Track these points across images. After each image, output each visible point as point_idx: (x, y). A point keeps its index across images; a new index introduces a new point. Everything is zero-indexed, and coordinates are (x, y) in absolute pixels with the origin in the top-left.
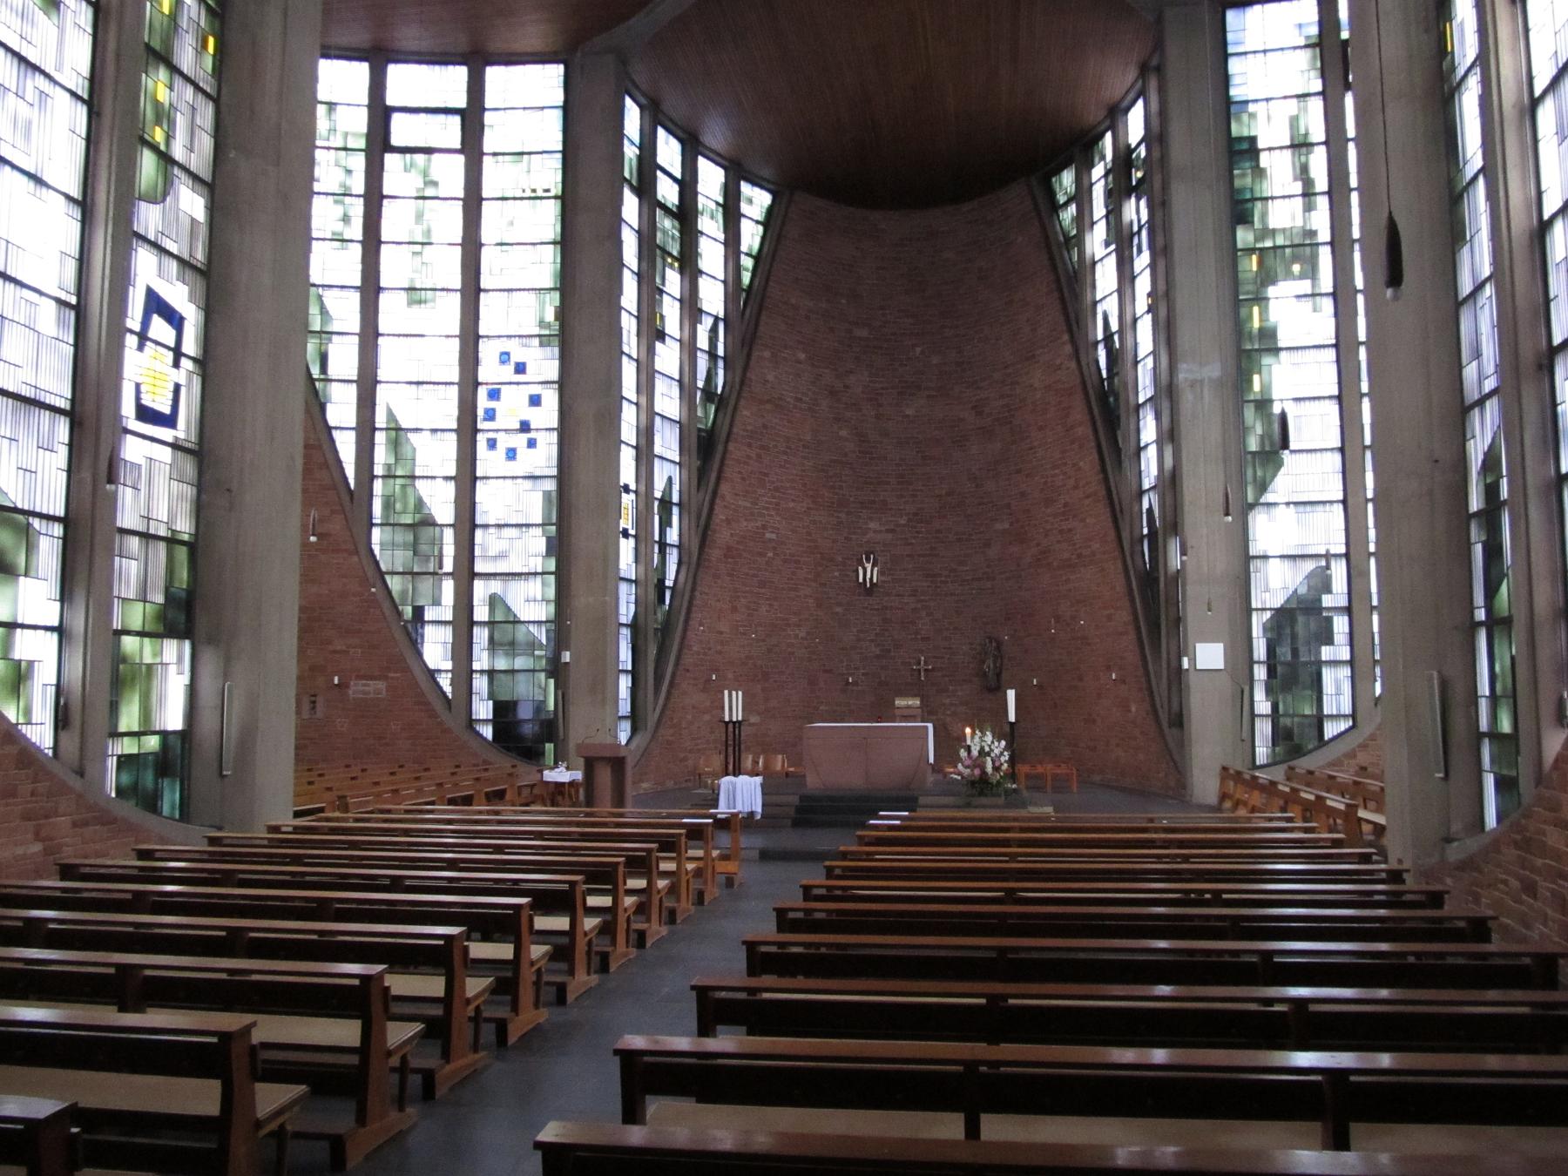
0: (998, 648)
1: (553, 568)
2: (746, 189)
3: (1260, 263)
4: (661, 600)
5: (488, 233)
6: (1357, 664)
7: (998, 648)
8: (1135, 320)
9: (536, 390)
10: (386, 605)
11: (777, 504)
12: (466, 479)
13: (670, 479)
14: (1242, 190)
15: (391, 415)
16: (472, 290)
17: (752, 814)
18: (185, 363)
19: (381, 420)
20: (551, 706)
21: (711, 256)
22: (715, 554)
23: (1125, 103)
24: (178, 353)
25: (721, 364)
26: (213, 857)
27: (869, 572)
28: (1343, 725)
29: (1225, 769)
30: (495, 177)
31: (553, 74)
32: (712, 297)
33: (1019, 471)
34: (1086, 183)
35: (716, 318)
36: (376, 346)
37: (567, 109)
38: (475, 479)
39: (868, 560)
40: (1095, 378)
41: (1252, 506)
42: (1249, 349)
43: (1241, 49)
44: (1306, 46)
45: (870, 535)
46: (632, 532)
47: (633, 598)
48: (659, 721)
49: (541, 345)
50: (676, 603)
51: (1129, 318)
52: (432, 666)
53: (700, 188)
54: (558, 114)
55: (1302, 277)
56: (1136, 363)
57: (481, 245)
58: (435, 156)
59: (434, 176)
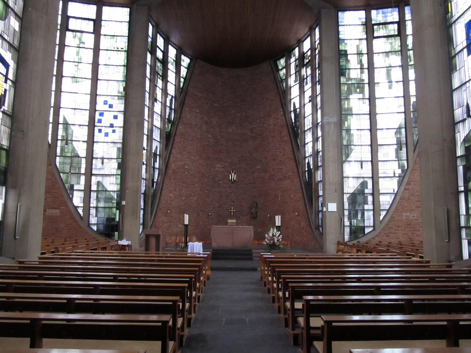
0: (257, 205)
1: (120, 173)
2: (183, 57)
3: (348, 88)
5: (102, 60)
6: (375, 211)
7: (257, 205)
8: (304, 105)
9: (116, 114)
10: (60, 184)
12: (91, 142)
13: (157, 147)
14: (342, 66)
15: (65, 119)
16: (95, 79)
18: (9, 82)
19: (61, 120)
20: (117, 219)
21: (171, 76)
22: (170, 172)
23: (303, 39)
24: (6, 78)
25: (173, 111)
26: (20, 268)
27: (233, 176)
28: (371, 229)
29: (339, 242)
30: (104, 43)
31: (126, 11)
32: (171, 90)
33: (265, 150)
34: (289, 63)
35: (172, 96)
36: (60, 95)
37: (130, 23)
38: (94, 142)
39: (233, 172)
40: (291, 122)
41: (345, 161)
42: (343, 114)
43: (343, 24)
44: (362, 25)
46: (145, 163)
49: (118, 99)
51: (303, 104)
52: (76, 205)
53: (169, 55)
54: (127, 24)
55: (360, 93)
57: (99, 65)
58: (84, 34)
59: (83, 40)
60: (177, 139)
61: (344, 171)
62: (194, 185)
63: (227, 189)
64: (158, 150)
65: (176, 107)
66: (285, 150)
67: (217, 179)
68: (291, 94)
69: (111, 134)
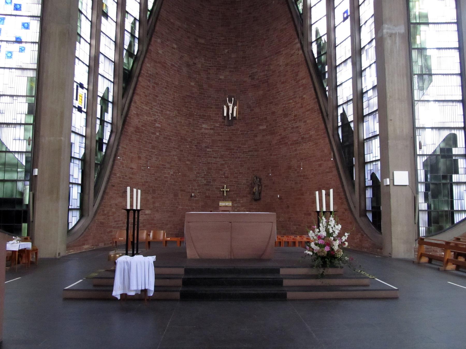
0: (260, 181)
4: (101, 149)
7: (260, 181)
8: (335, 27)
11: (162, 111)
13: (108, 89)
17: (145, 291)
22: (131, 129)
25: (137, 41)
27: (231, 109)
33: (271, 103)
35: (135, 19)
39: (230, 101)
40: (312, 58)
45: (203, 130)
47: (84, 145)
48: (96, 211)
50: (109, 151)
51: (332, 26)
56: (335, 47)
60: (143, 82)
61: (416, 117)
62: (170, 152)
63: (218, 160)
64: (111, 95)
65: (141, 35)
66: (304, 98)
67: (204, 145)
68: (311, 18)
69: (16, 54)
